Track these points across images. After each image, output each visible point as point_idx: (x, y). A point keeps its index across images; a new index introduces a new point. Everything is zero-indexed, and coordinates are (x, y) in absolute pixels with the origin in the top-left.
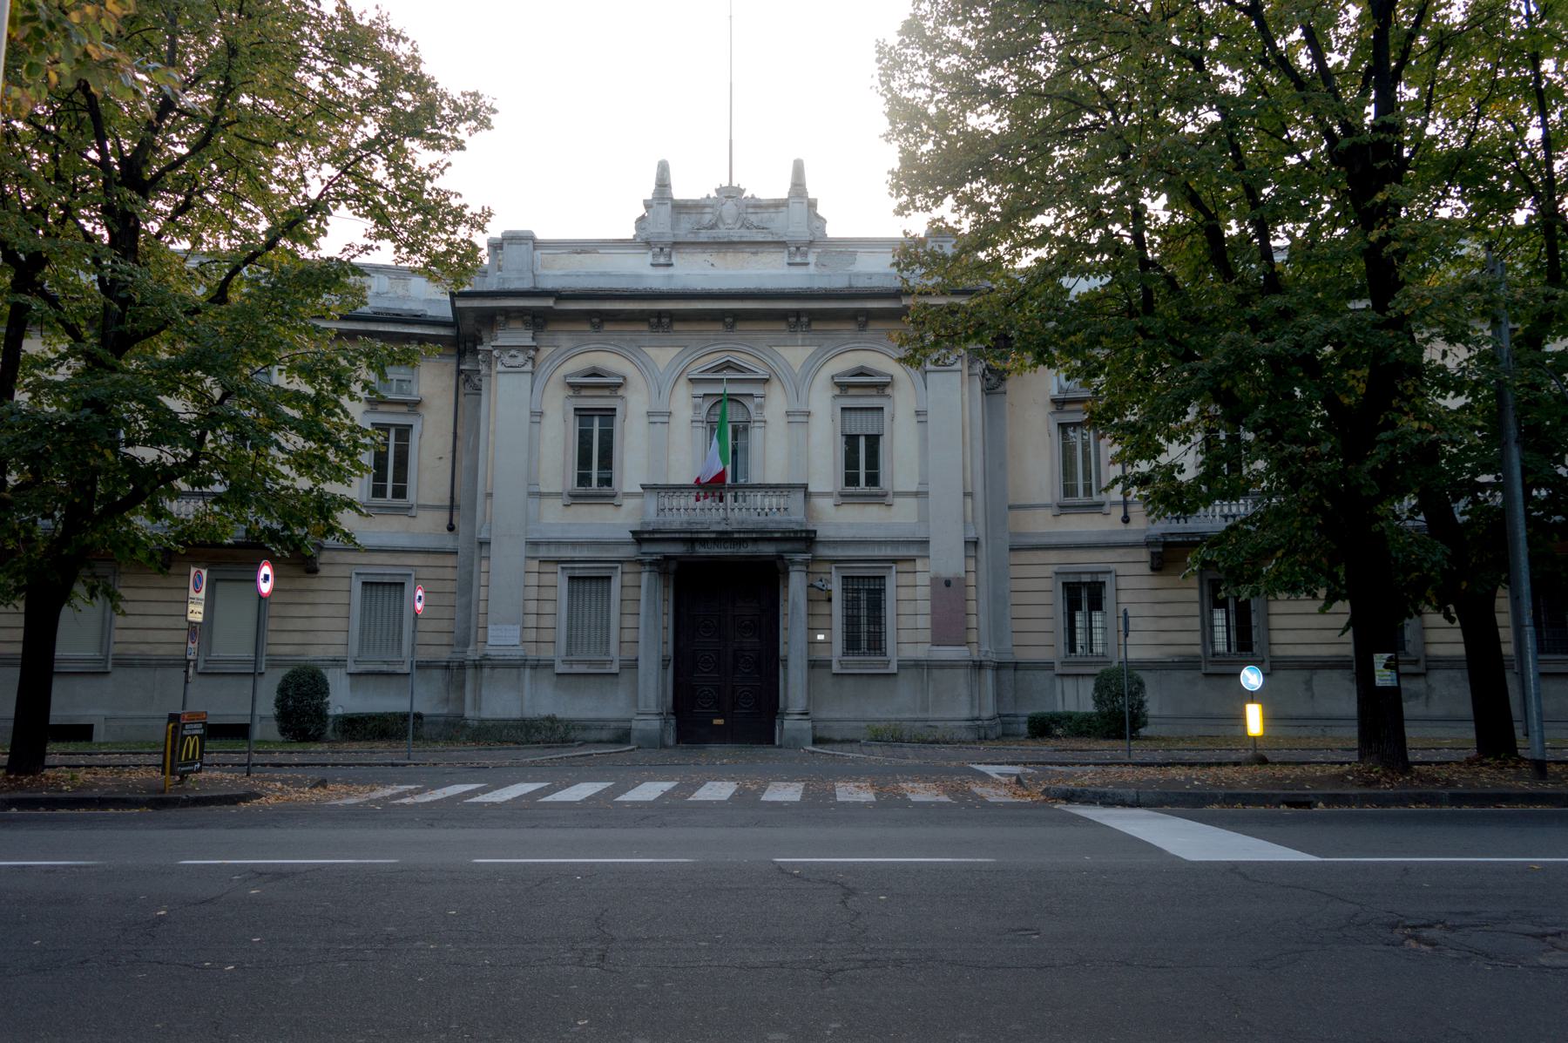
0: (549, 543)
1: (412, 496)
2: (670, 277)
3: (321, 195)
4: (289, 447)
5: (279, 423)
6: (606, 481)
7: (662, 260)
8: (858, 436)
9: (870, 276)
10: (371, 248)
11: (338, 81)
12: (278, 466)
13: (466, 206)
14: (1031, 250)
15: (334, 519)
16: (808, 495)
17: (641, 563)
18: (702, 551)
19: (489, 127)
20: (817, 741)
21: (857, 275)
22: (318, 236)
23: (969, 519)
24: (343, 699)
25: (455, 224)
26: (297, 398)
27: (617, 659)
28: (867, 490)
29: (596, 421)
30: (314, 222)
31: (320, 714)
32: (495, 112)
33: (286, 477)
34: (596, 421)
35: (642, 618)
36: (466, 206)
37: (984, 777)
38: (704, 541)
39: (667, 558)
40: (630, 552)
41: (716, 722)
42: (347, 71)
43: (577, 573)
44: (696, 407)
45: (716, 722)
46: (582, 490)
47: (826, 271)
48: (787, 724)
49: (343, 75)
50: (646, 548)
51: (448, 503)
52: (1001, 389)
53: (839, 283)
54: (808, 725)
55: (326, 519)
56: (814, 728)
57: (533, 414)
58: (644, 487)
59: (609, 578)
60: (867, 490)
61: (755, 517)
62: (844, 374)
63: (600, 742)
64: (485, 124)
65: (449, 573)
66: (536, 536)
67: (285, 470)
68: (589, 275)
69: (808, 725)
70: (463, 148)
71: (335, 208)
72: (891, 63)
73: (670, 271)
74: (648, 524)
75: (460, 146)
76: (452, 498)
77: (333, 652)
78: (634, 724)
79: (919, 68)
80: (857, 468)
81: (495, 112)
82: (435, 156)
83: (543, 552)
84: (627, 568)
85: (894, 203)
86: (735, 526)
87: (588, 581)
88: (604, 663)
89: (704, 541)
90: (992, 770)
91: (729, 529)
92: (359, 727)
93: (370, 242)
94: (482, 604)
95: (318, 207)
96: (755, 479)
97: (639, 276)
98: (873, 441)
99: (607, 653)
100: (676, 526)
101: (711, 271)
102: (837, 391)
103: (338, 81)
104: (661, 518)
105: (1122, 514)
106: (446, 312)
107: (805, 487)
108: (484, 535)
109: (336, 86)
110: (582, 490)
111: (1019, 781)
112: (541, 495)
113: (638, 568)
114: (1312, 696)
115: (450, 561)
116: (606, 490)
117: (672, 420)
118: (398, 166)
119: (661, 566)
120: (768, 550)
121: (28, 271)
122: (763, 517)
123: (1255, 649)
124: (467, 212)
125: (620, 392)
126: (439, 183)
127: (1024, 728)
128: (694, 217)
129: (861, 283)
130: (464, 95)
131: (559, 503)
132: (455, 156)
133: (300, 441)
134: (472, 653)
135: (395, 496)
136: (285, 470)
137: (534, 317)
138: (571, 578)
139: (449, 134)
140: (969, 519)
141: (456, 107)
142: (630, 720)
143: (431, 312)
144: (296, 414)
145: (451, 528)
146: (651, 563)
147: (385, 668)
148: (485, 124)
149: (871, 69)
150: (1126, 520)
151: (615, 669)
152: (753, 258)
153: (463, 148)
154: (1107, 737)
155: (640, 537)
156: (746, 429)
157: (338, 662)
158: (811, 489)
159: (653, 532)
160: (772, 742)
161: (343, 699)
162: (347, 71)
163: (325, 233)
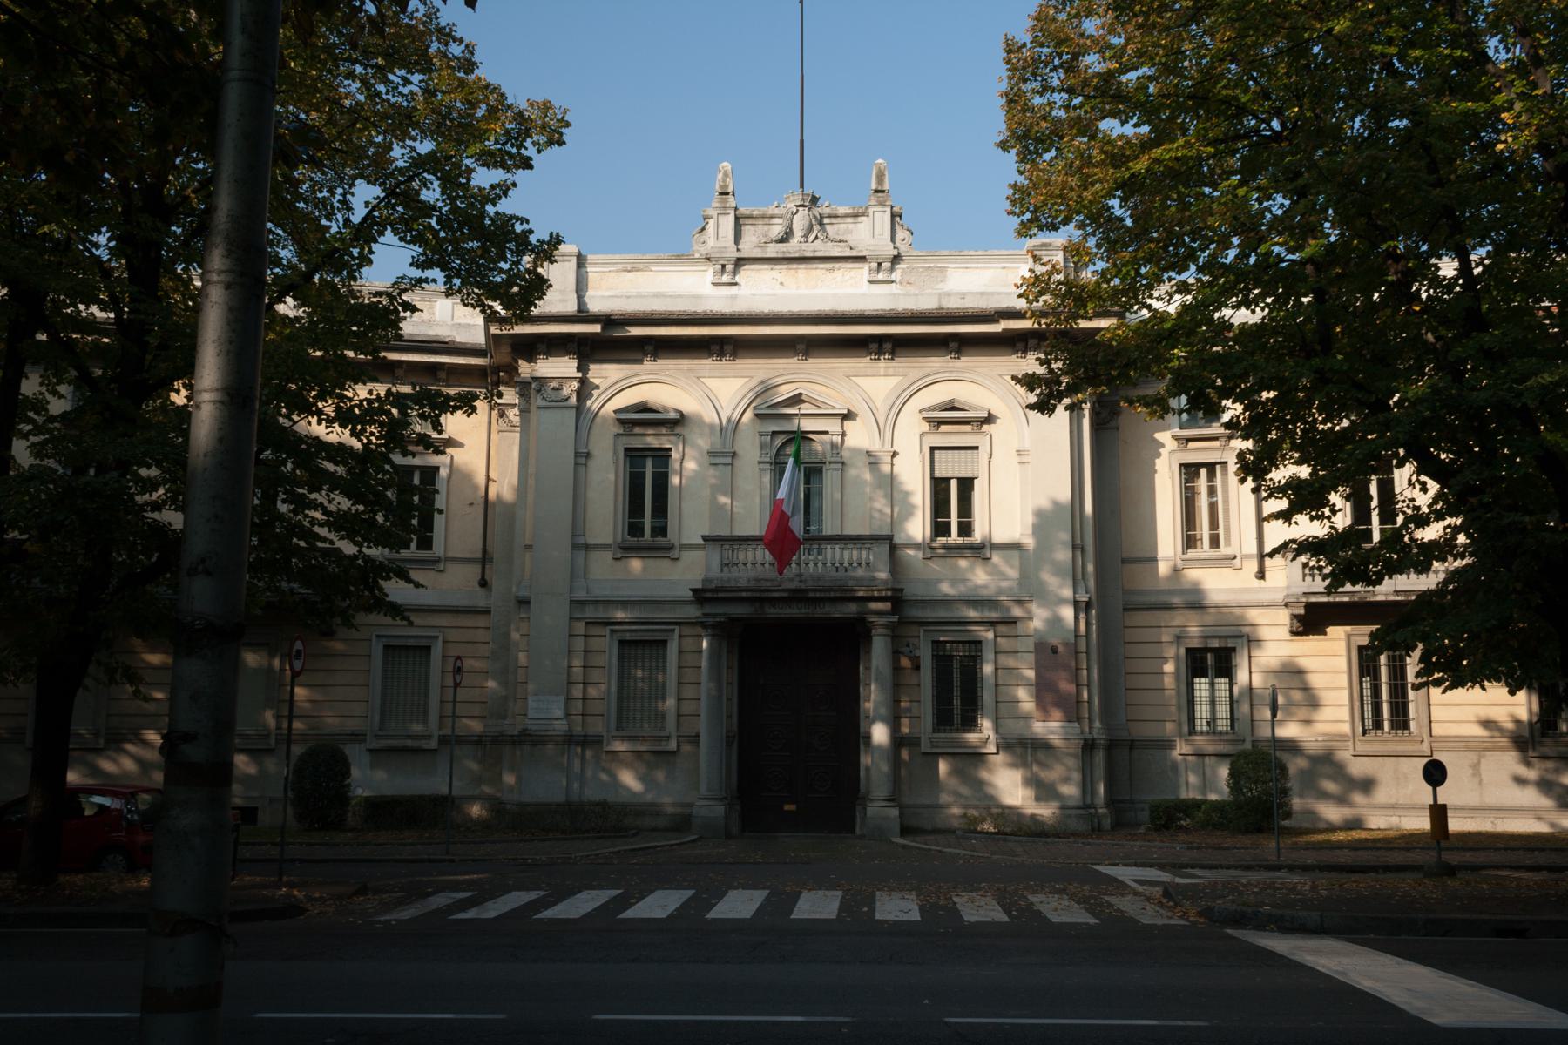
0: (596, 602)
1: (438, 549)
2: (734, 297)
3: (364, 220)
4: (332, 508)
5: (319, 479)
6: (660, 531)
7: (725, 278)
8: (948, 480)
9: (963, 296)
10: (426, 280)
11: (381, 88)
12: (316, 529)
13: (531, 232)
14: (1173, 274)
15: (381, 589)
16: (893, 548)
17: (703, 625)
18: (772, 612)
19: (561, 143)
20: (906, 831)
21: (948, 295)
22: (360, 266)
23: (1080, 576)
24: (368, 780)
25: (520, 253)
26: (338, 452)
27: (674, 734)
28: (960, 540)
29: (649, 463)
30: (355, 252)
31: (341, 796)
32: (568, 125)
33: (324, 540)
34: (649, 463)
35: (704, 687)
36: (531, 232)
37: (1119, 886)
38: (773, 601)
39: (733, 620)
40: (693, 612)
41: (787, 807)
42: (391, 76)
43: (628, 637)
44: (762, 446)
45: (787, 807)
46: (633, 541)
47: (912, 290)
48: (870, 811)
49: (386, 81)
50: (709, 609)
51: (479, 555)
52: (1112, 424)
53: (926, 303)
54: (894, 812)
55: (371, 590)
56: (901, 815)
57: (577, 454)
58: (705, 538)
59: (664, 643)
60: (960, 540)
61: (834, 573)
62: (933, 409)
63: (654, 830)
64: (556, 140)
65: (481, 635)
66: (581, 594)
67: (323, 532)
68: (640, 296)
69: (894, 812)
70: (530, 167)
71: (381, 233)
72: (1022, 65)
73: (733, 290)
74: (711, 581)
75: (527, 164)
76: (484, 550)
77: (352, 725)
78: (695, 810)
79: (1055, 69)
80: (960, 523)
81: (568, 125)
82: (497, 175)
83: (590, 613)
84: (687, 630)
85: (1015, 222)
86: (810, 584)
87: (641, 646)
88: (659, 739)
89: (773, 601)
90: (1124, 873)
91: (803, 586)
92: (384, 811)
93: (416, 273)
94: (521, 671)
95: (366, 233)
96: (828, 530)
97: (697, 297)
98: (966, 485)
99: (663, 728)
100: (743, 583)
101: (780, 291)
102: (925, 427)
103: (381, 88)
104: (726, 574)
105: (1255, 569)
106: (479, 338)
107: (890, 538)
108: (523, 593)
109: (379, 94)
110: (633, 541)
111: (1166, 894)
112: (587, 547)
113: (699, 630)
114: (1480, 782)
115: (481, 621)
116: (660, 541)
117: (737, 463)
118: (453, 181)
119: (723, 631)
120: (852, 609)
121: (30, 306)
122: (841, 573)
123: (1413, 724)
124: (533, 239)
125: (678, 430)
126: (505, 206)
127: (1145, 816)
128: (761, 229)
129: (953, 304)
130: (532, 105)
131: (608, 555)
132: (520, 176)
133: (345, 504)
134: (512, 726)
135: (418, 548)
136: (323, 532)
137: (579, 345)
138: (622, 643)
139: (514, 150)
140: (1080, 576)
141: (520, 117)
142: (691, 805)
143: (461, 338)
144: (341, 470)
145: (483, 583)
146: (713, 626)
147: (409, 743)
148: (556, 140)
149: (997, 78)
150: (1261, 575)
151: (433, 744)
152: (830, 276)
153: (530, 167)
154: (1247, 831)
155: (701, 596)
156: (820, 471)
157: (357, 737)
158: (897, 540)
159: (717, 590)
160: (853, 832)
161: (368, 780)
162: (391, 76)
163: (370, 262)
